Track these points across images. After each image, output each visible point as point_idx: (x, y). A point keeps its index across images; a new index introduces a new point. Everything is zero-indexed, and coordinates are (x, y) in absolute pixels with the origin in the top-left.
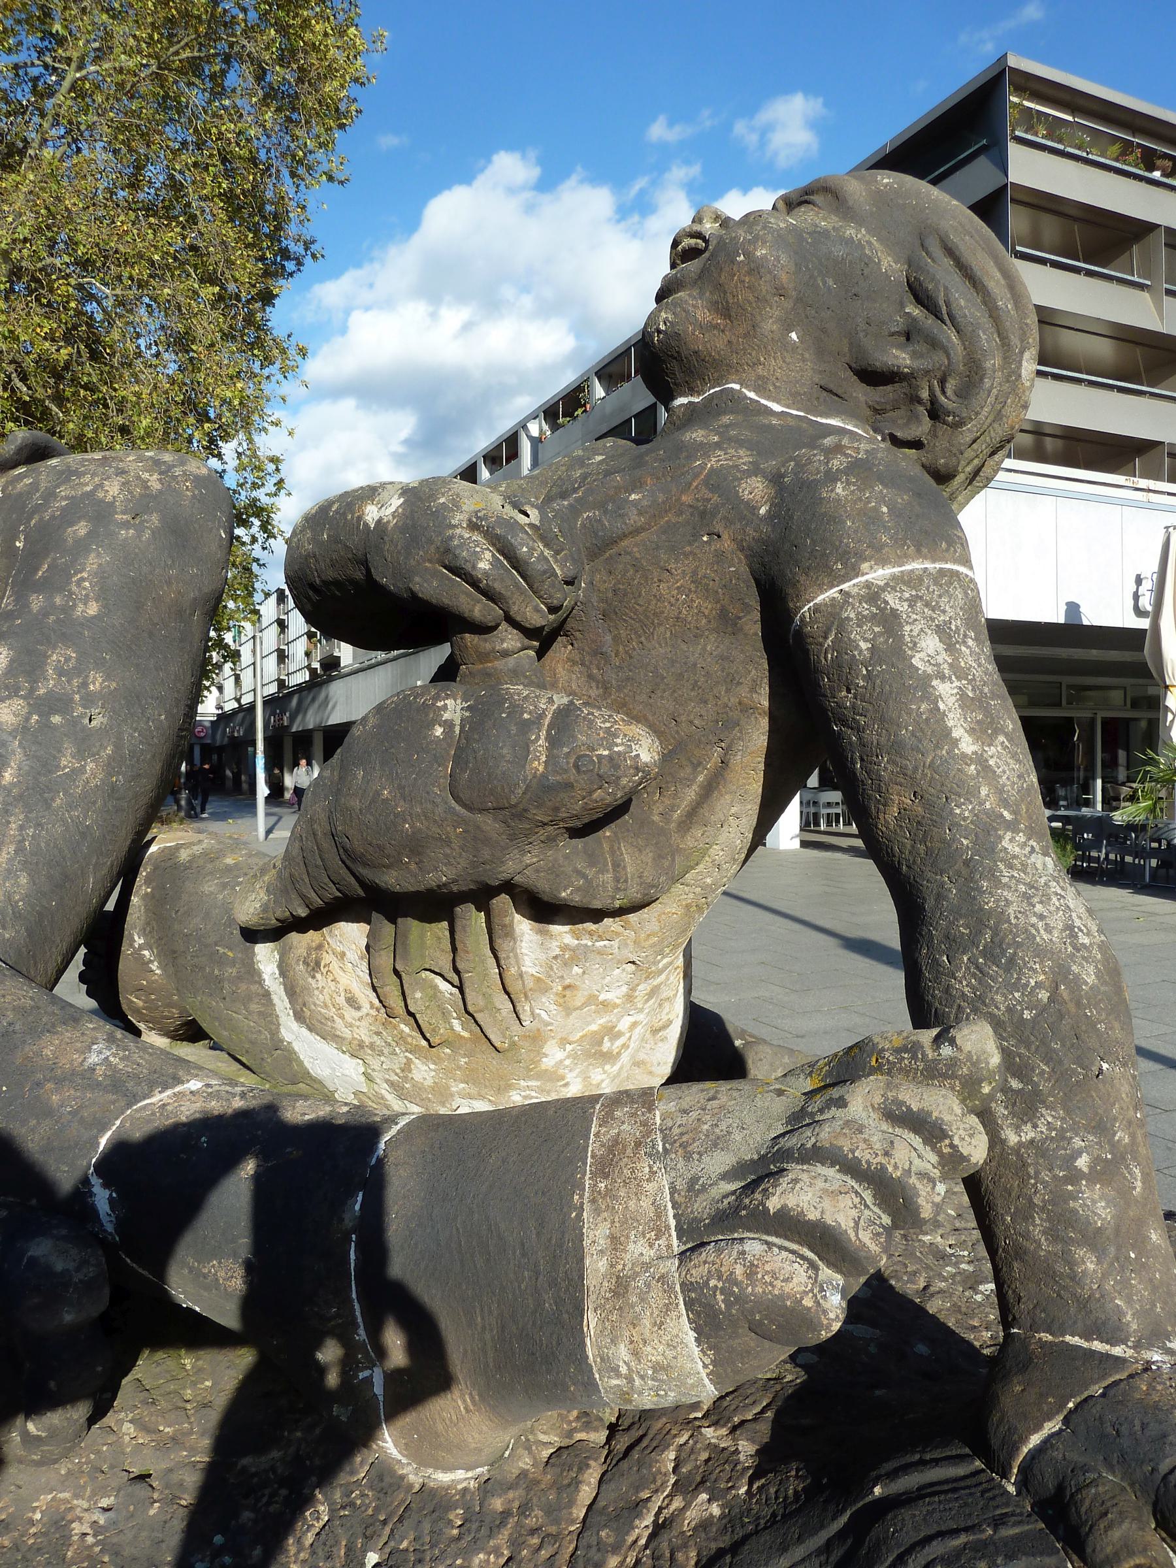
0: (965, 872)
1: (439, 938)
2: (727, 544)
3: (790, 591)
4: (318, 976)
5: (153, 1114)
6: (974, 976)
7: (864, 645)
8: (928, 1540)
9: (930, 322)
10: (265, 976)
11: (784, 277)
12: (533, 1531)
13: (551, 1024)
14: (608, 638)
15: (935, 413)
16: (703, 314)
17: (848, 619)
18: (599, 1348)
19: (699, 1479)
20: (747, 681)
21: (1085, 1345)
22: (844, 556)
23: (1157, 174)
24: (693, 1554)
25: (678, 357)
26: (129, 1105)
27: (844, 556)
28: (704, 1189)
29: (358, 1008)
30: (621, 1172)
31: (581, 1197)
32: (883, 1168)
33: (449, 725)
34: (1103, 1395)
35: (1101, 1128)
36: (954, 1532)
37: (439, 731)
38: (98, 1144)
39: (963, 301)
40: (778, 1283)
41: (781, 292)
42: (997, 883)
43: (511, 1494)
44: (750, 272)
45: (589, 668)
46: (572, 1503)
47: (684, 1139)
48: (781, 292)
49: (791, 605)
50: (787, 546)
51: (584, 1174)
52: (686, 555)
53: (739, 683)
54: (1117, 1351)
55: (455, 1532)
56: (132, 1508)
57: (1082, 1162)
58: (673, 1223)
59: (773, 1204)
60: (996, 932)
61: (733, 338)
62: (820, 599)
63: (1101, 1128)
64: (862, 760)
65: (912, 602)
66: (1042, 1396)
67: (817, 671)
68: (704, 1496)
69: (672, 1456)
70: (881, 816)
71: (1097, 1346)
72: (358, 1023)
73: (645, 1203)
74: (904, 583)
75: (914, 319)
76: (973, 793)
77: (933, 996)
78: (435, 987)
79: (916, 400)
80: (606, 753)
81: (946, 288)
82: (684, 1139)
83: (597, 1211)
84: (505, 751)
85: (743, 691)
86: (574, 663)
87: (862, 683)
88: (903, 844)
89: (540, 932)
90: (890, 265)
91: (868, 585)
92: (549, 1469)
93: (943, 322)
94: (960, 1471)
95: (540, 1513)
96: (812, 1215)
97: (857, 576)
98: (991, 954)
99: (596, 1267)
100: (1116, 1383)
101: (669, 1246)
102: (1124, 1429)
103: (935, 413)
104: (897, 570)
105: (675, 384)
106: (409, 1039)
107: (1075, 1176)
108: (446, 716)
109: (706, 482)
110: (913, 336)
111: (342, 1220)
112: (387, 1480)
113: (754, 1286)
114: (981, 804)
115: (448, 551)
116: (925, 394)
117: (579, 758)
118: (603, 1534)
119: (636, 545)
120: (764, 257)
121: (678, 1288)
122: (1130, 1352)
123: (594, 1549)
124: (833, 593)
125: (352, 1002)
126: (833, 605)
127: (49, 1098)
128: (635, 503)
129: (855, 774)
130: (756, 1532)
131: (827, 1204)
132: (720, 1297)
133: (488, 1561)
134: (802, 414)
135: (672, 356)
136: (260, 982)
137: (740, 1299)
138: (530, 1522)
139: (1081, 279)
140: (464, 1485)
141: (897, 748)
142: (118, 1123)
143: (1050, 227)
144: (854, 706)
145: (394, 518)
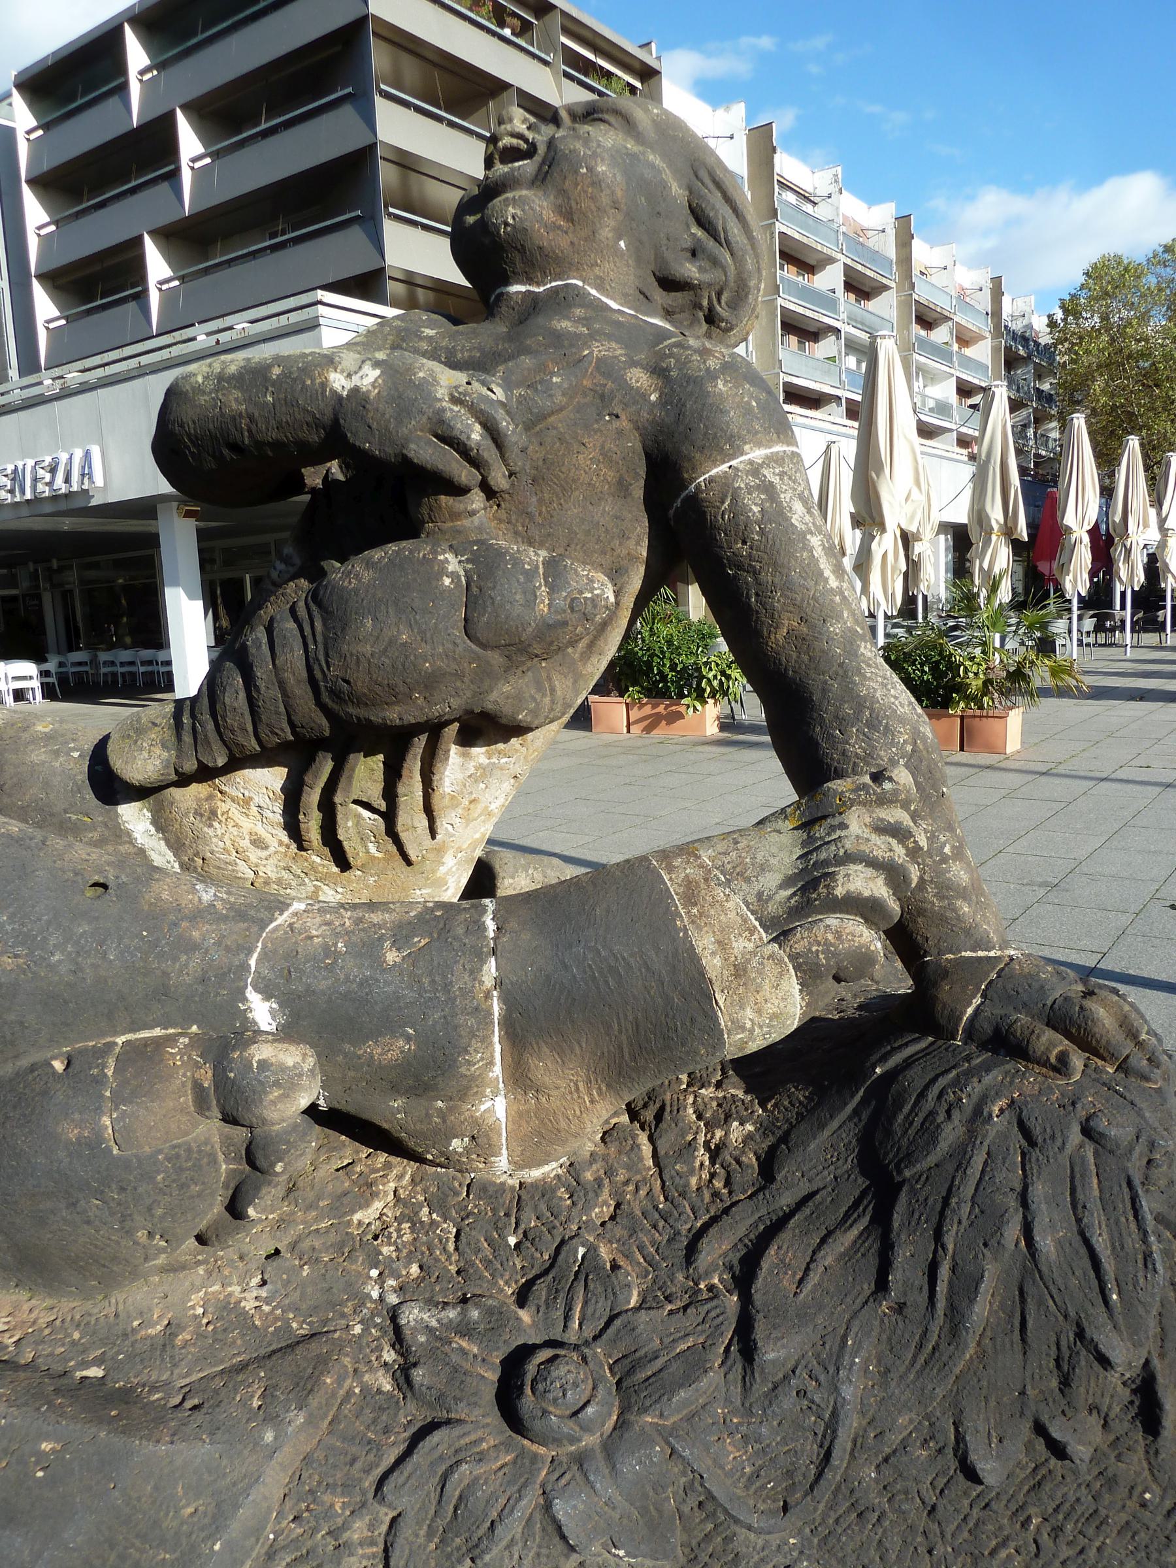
0: (841, 672)
1: (373, 770)
2: (624, 423)
3: (686, 464)
4: (216, 824)
5: (286, 933)
6: (863, 741)
7: (756, 509)
8: (933, 1081)
9: (711, 243)
10: (135, 835)
11: (619, 193)
12: (627, 1183)
13: (453, 836)
14: (534, 499)
15: (711, 319)
16: (549, 215)
17: (739, 488)
18: (730, 1015)
19: (722, 1116)
20: (634, 536)
21: (974, 955)
22: (731, 439)
23: (507, 32)
24: (751, 1155)
25: (522, 250)
26: (263, 929)
27: (731, 439)
28: (770, 898)
29: (266, 848)
30: (704, 899)
31: (682, 921)
32: (893, 860)
33: (454, 576)
34: (999, 976)
35: (950, 828)
36: (948, 1071)
37: (447, 581)
38: (249, 965)
39: (735, 230)
40: (856, 939)
41: (616, 206)
42: (864, 677)
43: (594, 1167)
44: (593, 184)
45: (515, 525)
46: (641, 1159)
47: (738, 870)
48: (616, 206)
49: (686, 476)
50: (681, 428)
51: (677, 907)
52: (596, 431)
53: (628, 538)
54: (992, 954)
55: (569, 1202)
56: (285, 1276)
57: (947, 850)
58: (757, 924)
59: (839, 892)
60: (872, 711)
61: (575, 240)
62: (713, 472)
63: (950, 828)
64: (757, 595)
65: (782, 475)
66: (964, 988)
67: (713, 527)
68: (736, 1124)
69: (691, 1111)
70: (772, 637)
71: (981, 954)
72: (264, 862)
73: (732, 915)
74: (776, 462)
75: (699, 240)
76: (839, 617)
77: (832, 759)
78: (359, 816)
79: (697, 306)
80: (589, 595)
81: (724, 217)
82: (738, 870)
83: (699, 928)
84: (518, 597)
85: (631, 544)
86: (500, 521)
87: (757, 538)
88: (790, 656)
89: (464, 755)
90: (677, 191)
91: (751, 462)
92: (609, 1145)
93: (721, 244)
94: (923, 1044)
95: (624, 1171)
96: (866, 894)
97: (742, 454)
98: (872, 724)
99: (713, 965)
100: (1002, 969)
101: (761, 939)
102: (1021, 991)
103: (711, 319)
104: (768, 451)
105: (513, 272)
106: (320, 869)
107: (945, 859)
108: (450, 568)
109: (597, 368)
110: (699, 255)
111: (481, 983)
112: (491, 1190)
113: (842, 943)
114: (845, 623)
115: (442, 422)
116: (705, 303)
117: (573, 600)
118: (677, 1167)
119: (561, 421)
120: (604, 173)
121: (786, 959)
122: (999, 953)
123: (678, 1178)
124: (724, 467)
125: (259, 843)
126: (726, 477)
127: (191, 935)
128: (559, 385)
129: (749, 605)
130: (792, 1127)
131: (871, 885)
132: (821, 956)
133: (602, 1211)
134: (632, 312)
135: (516, 248)
136: (131, 841)
137: (834, 954)
138: (621, 1177)
139: (443, 128)
140: (554, 1173)
141: (788, 587)
142: (260, 945)
143: (411, 69)
144: (750, 555)
145: (374, 388)
